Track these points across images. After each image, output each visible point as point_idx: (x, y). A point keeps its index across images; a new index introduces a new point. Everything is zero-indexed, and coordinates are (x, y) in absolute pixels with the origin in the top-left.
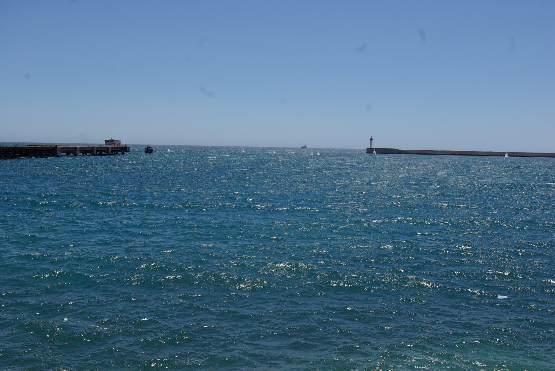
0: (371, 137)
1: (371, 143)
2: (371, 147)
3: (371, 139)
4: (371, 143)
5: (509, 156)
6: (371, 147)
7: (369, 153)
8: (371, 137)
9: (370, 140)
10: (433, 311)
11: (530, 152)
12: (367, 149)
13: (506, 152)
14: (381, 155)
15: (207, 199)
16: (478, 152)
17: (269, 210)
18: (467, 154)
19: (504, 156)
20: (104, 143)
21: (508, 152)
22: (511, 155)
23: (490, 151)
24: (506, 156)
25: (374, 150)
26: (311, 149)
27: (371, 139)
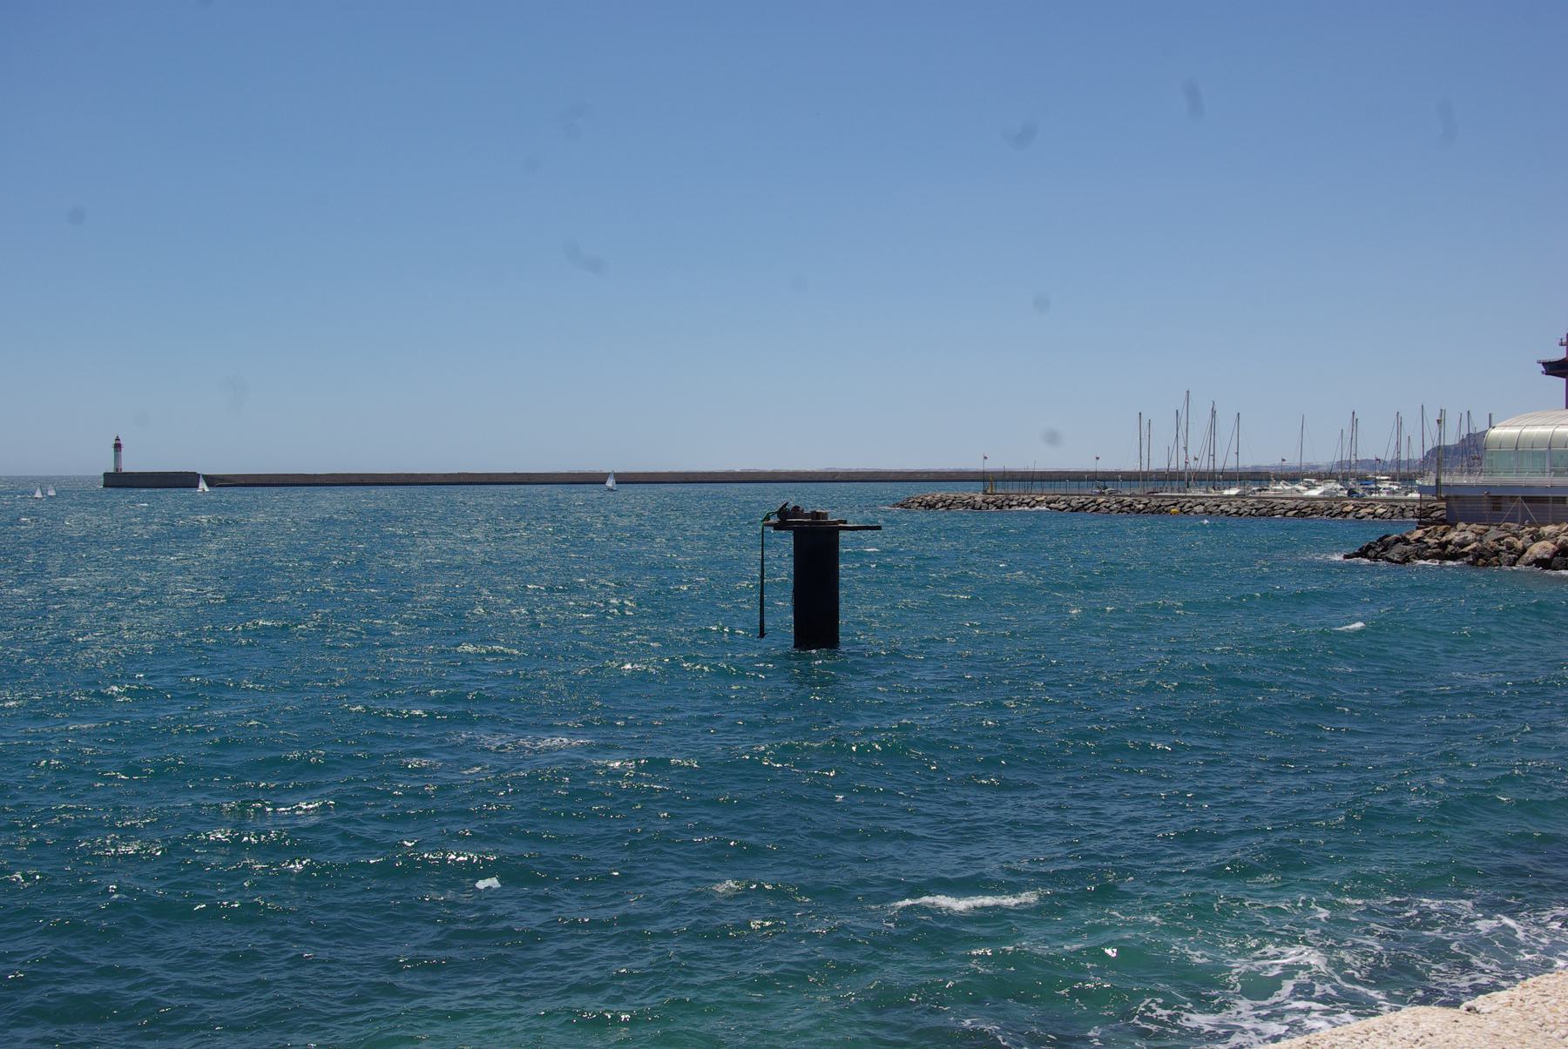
0: (118, 439)
1: (117, 458)
2: (117, 469)
3: (118, 447)
4: (117, 458)
5: (617, 483)
6: (117, 469)
7: (110, 487)
8: (118, 439)
9: (113, 449)
10: (326, 939)
11: (565, 471)
12: (106, 475)
13: (610, 471)
14: (1470, 487)
15: (812, 679)
16: (428, 475)
17: (1552, 705)
18: (759, 479)
19: (604, 483)
20: (1374, 459)
21: (615, 474)
22: (624, 479)
23: (460, 472)
24: (610, 483)
25: (201, 479)
26: (86, 480)
27: (118, 447)
